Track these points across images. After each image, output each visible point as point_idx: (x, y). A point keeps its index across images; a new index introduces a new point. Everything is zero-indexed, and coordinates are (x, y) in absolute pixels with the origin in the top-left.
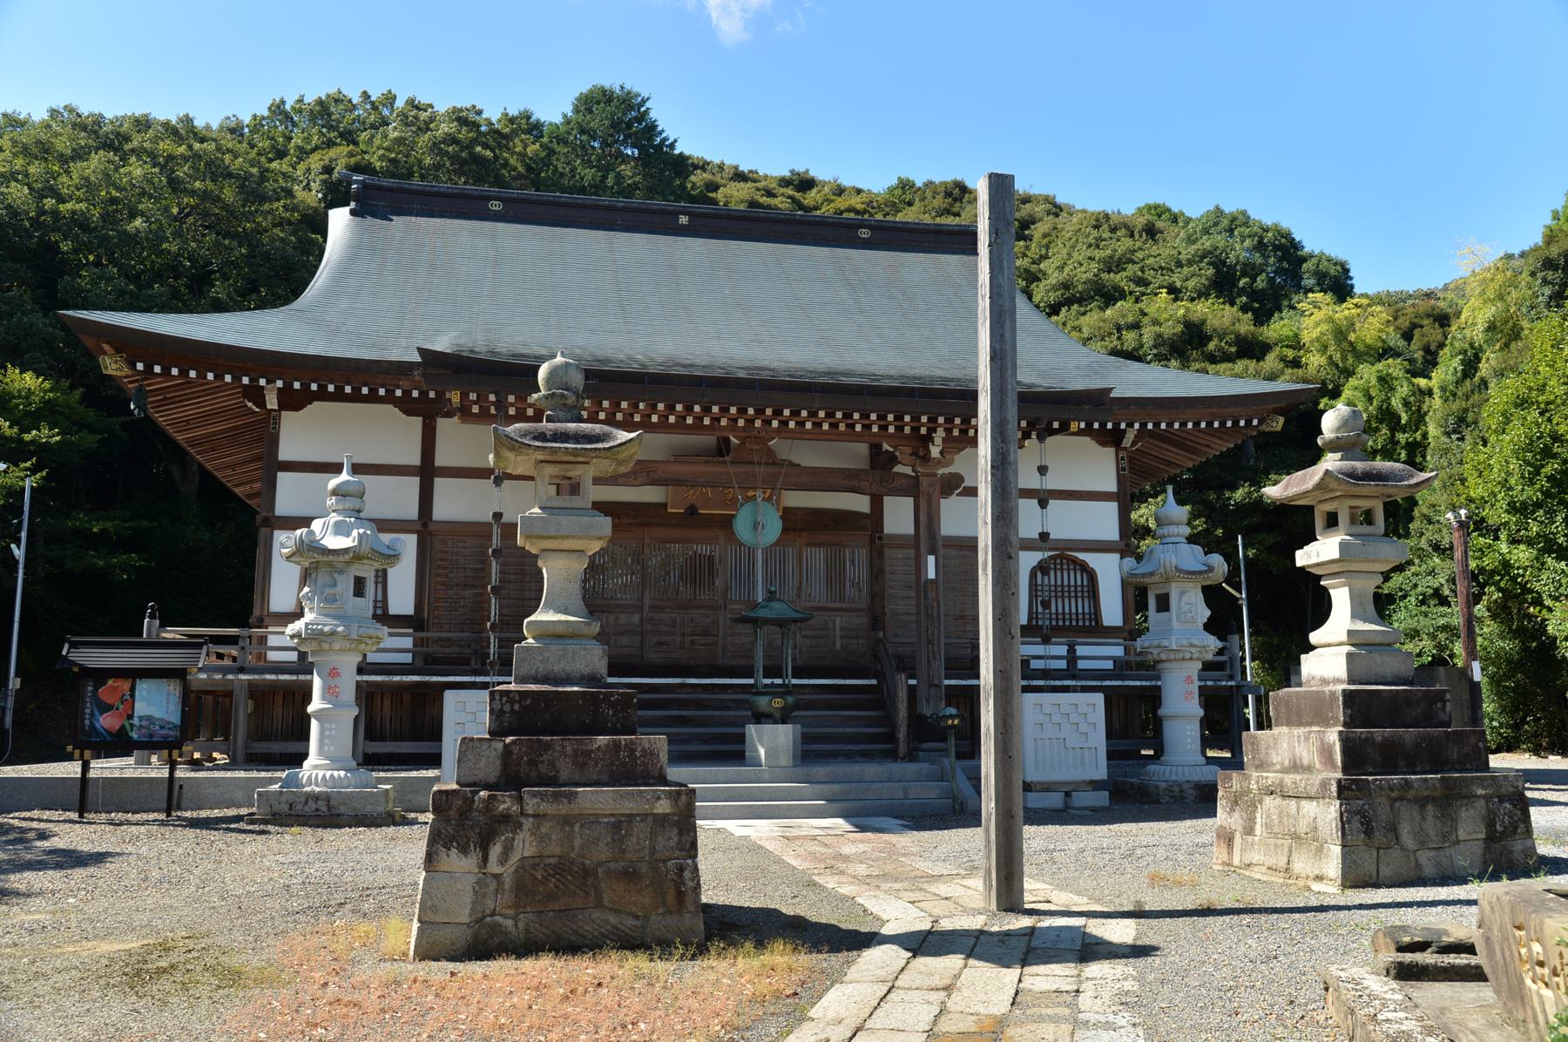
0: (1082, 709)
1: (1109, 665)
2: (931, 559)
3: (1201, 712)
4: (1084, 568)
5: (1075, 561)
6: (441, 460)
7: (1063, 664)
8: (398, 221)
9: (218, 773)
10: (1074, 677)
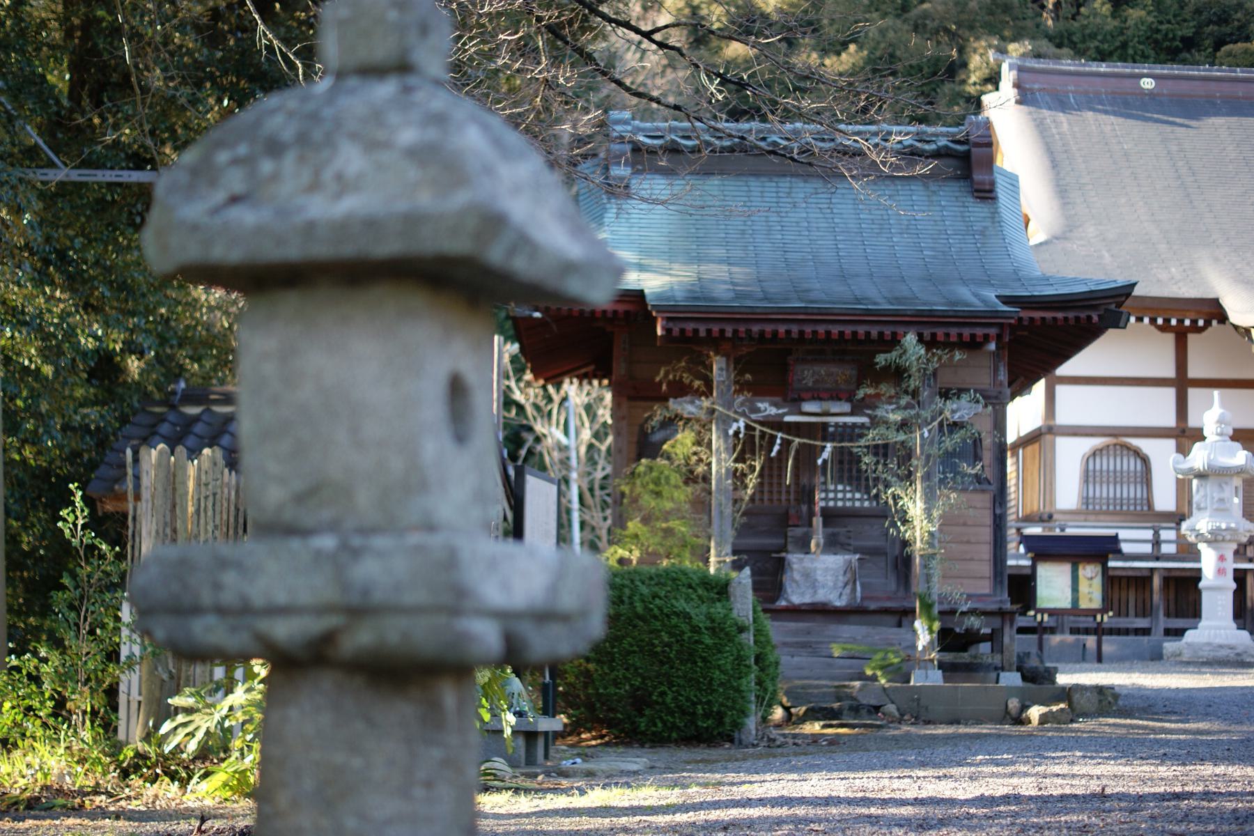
3: (1234, 586)
4: (1137, 453)
5: (1128, 448)
6: (1193, 372)
7: (1147, 549)
8: (715, 181)
9: (811, 748)
10: (1157, 559)
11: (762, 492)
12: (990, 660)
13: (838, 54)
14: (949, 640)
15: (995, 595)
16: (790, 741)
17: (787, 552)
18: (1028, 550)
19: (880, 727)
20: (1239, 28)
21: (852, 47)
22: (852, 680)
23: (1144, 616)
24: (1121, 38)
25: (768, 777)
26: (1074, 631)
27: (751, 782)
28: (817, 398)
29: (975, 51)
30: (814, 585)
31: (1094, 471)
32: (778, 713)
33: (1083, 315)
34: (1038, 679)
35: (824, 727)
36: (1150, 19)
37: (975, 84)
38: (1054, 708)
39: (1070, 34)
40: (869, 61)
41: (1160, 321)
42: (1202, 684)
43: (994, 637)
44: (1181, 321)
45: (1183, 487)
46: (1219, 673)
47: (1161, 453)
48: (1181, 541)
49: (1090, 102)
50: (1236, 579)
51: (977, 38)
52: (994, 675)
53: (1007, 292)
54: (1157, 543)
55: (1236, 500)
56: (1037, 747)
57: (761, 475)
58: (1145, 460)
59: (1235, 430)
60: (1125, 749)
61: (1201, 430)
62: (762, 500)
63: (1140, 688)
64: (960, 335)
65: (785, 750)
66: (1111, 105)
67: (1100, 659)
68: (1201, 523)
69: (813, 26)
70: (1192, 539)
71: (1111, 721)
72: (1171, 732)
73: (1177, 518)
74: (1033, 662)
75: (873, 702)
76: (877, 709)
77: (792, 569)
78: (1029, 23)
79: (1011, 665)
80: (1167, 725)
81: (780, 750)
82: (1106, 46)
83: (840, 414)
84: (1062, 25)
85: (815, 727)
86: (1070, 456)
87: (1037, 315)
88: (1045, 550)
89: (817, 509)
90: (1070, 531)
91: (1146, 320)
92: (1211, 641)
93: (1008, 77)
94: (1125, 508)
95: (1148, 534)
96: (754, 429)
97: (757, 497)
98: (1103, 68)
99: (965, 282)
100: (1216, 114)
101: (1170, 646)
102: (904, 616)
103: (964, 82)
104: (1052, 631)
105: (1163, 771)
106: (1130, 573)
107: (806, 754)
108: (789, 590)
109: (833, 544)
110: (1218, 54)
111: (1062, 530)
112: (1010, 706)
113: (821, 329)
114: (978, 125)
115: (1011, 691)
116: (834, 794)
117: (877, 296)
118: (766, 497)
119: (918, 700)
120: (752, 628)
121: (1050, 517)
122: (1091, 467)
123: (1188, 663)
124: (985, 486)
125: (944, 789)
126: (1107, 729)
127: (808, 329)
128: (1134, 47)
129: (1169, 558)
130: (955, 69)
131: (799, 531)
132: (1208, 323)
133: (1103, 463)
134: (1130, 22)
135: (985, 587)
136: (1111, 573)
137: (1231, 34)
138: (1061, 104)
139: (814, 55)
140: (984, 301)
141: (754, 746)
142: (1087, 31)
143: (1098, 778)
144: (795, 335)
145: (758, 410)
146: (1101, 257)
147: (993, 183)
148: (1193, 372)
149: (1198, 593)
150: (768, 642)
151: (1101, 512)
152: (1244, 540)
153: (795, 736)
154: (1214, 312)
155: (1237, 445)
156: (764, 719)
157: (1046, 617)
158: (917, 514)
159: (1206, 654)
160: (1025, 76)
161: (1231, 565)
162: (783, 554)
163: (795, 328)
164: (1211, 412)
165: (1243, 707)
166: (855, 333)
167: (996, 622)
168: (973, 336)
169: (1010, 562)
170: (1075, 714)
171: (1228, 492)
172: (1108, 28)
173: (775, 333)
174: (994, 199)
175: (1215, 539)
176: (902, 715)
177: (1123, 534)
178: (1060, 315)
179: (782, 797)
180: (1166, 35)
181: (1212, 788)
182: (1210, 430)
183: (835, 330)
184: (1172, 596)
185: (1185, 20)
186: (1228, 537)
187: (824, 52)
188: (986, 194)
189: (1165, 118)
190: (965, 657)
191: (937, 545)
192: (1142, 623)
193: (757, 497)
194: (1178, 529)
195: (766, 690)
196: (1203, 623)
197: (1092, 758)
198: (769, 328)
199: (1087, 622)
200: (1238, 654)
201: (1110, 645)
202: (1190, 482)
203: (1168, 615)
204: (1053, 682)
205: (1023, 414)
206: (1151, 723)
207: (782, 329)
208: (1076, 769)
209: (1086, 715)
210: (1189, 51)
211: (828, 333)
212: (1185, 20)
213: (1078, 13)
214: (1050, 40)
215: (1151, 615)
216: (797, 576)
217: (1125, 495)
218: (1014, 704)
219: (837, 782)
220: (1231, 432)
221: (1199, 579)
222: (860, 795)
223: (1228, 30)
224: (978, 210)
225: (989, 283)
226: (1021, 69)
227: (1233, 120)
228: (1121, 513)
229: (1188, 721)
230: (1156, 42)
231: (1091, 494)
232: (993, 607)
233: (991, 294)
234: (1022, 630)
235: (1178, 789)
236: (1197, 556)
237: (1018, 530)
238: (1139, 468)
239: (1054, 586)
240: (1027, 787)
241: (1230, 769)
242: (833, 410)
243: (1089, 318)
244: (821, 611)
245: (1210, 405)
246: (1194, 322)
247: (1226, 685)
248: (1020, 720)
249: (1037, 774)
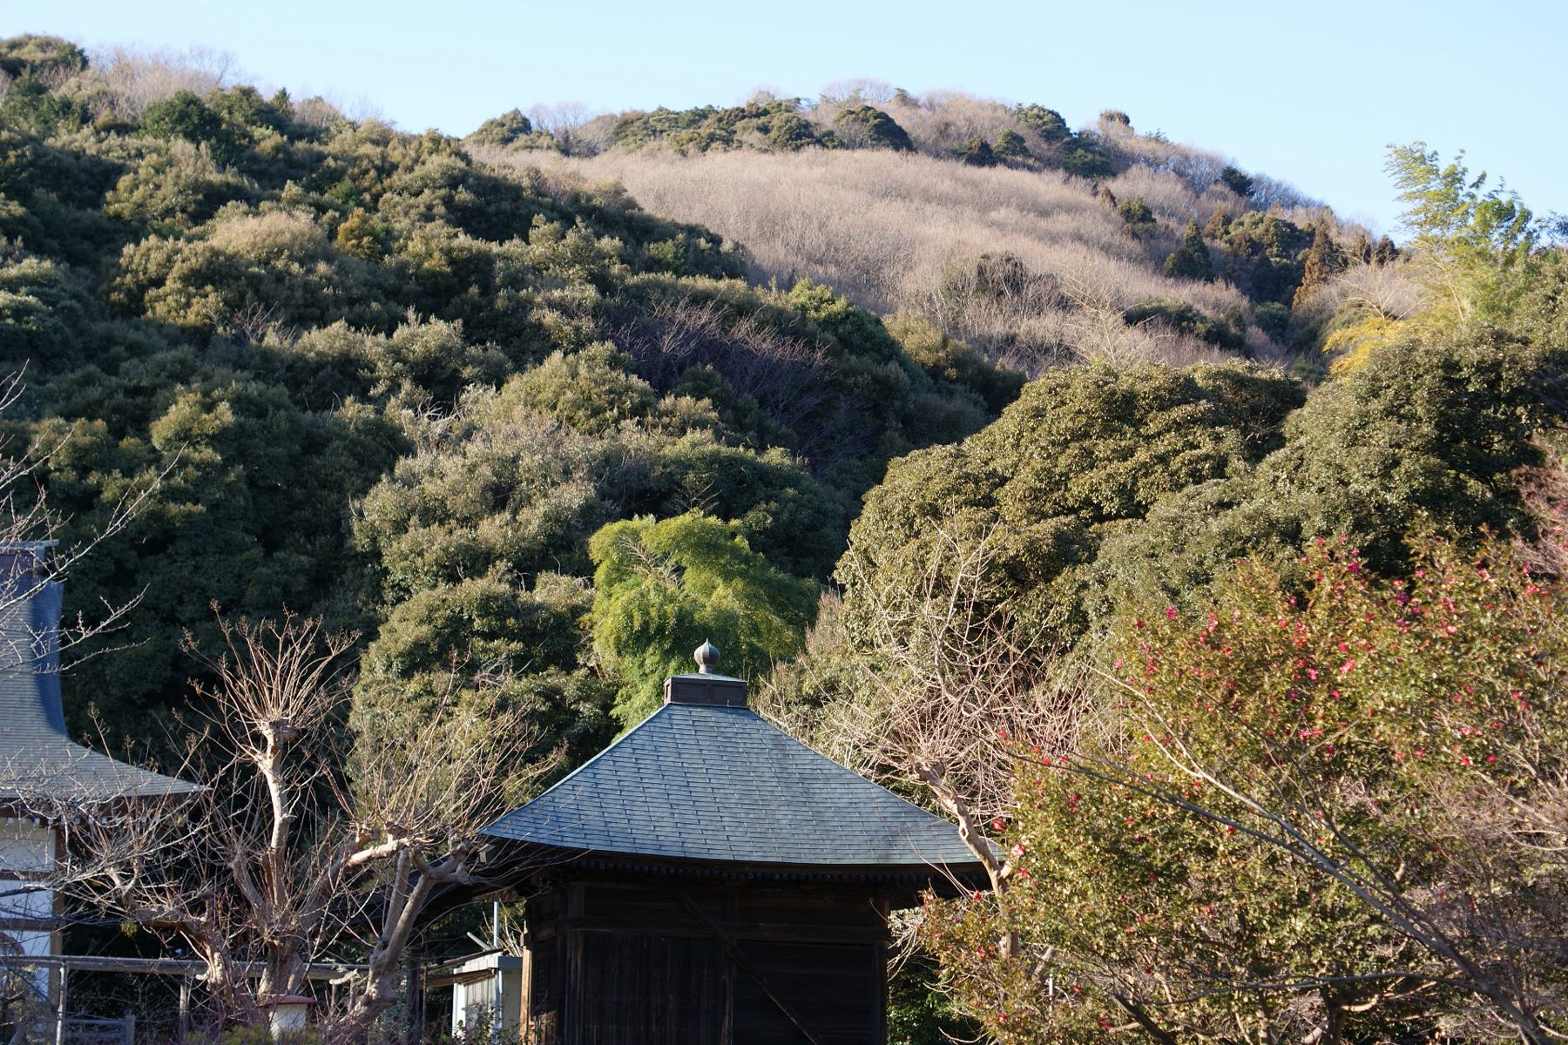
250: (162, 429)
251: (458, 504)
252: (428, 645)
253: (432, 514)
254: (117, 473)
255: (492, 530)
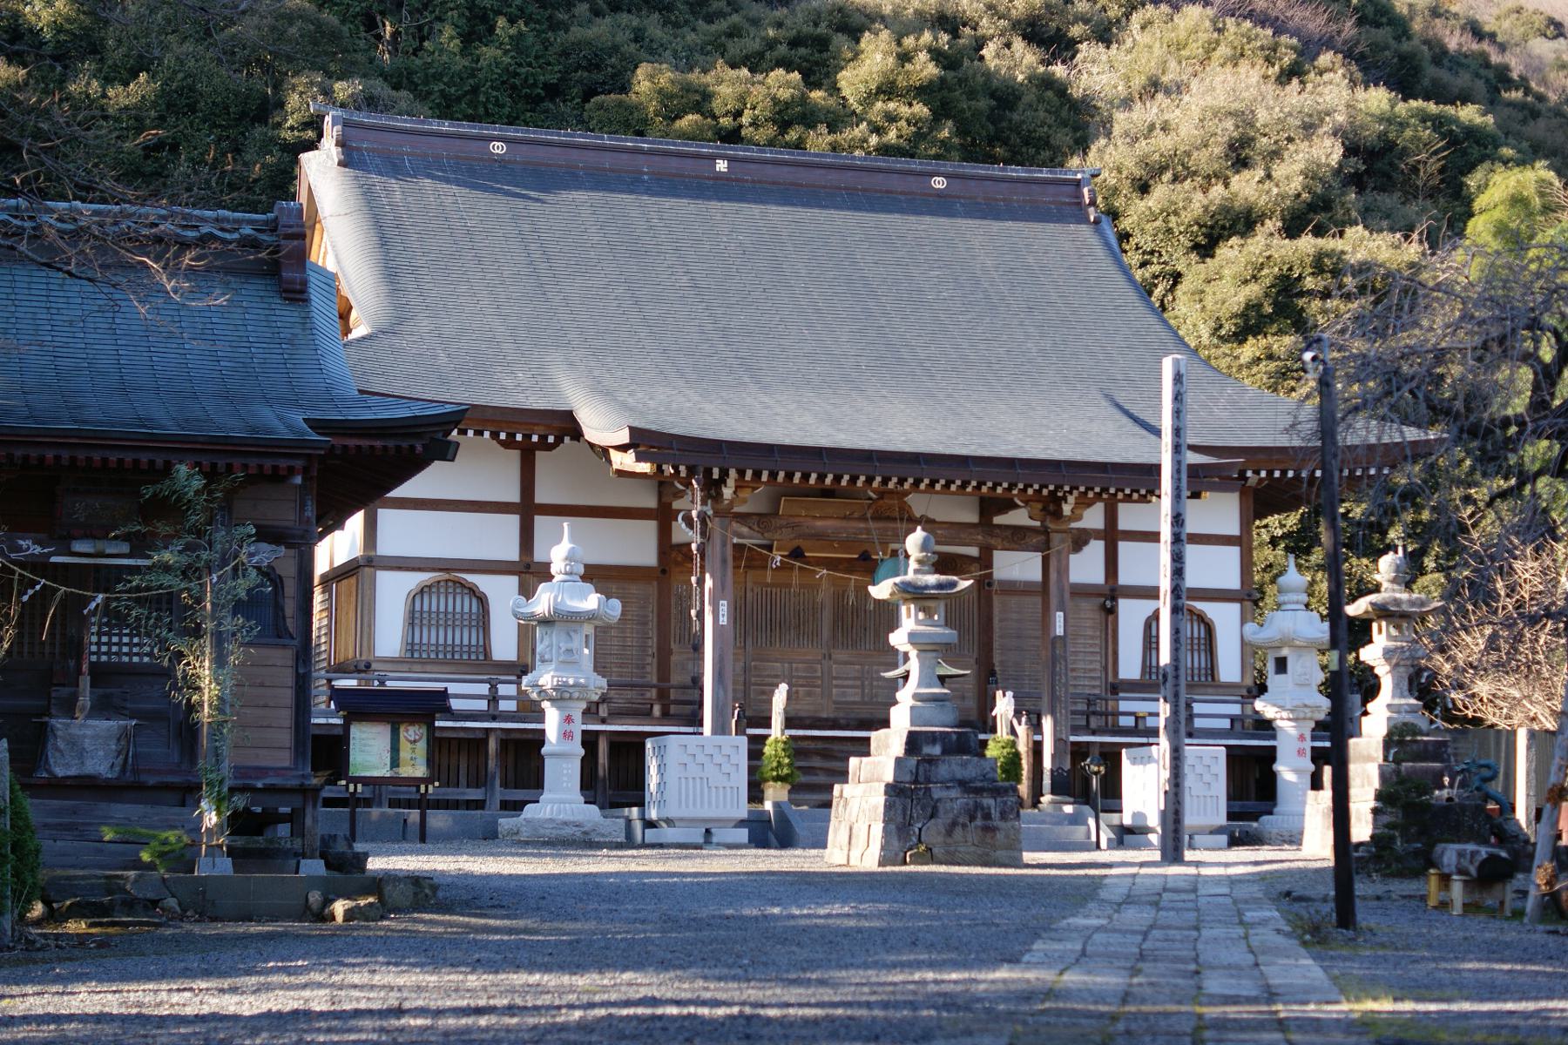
0: (1207, 761)
1: (1226, 724)
2: (1060, 616)
3: (582, 752)
4: (473, 591)
6: (541, 497)
7: (482, 705)
9: (76, 952)
10: (494, 718)
11: (21, 644)
12: (289, 845)
13: (126, 84)
14: (239, 823)
15: (296, 769)
16: (52, 943)
17: (50, 716)
18: (339, 707)
19: (157, 925)
20: (613, 76)
21: (143, 77)
22: (125, 869)
23: (477, 787)
24: (471, 81)
25: (29, 989)
26: (393, 803)
27: (12, 997)
28: (89, 535)
29: (294, 90)
30: (81, 754)
31: (422, 612)
32: (38, 909)
33: (405, 445)
34: (345, 868)
35: (91, 925)
36: (507, 60)
37: (292, 128)
38: (362, 903)
39: (411, 73)
40: (162, 94)
41: (503, 436)
42: (540, 870)
43: (295, 818)
44: (527, 437)
45: (527, 631)
46: (561, 856)
47: (500, 591)
48: (521, 697)
49: (429, 167)
50: (584, 744)
51: (296, 74)
52: (294, 862)
53: (317, 415)
54: (493, 699)
55: (586, 651)
56: (338, 949)
57: (20, 625)
58: (482, 600)
59: (587, 566)
60: (432, 954)
61: (548, 565)
62: (20, 653)
63: (468, 876)
64: (261, 467)
65: (47, 955)
66: (455, 172)
67: (423, 839)
68: (546, 678)
69: (94, 49)
70: (534, 696)
71: (427, 916)
72: (496, 930)
73: (520, 669)
74: (341, 847)
75: (151, 895)
76: (155, 903)
77: (55, 737)
78: (360, 57)
79: (313, 851)
80: (491, 922)
81: (40, 955)
82: (453, 90)
83: (116, 554)
84: (400, 59)
85: (76, 927)
86: (393, 594)
87: (352, 442)
88: (361, 706)
89: (85, 667)
90: (391, 685)
91: (487, 434)
92: (554, 816)
93: (331, 132)
94: (457, 656)
95: (484, 689)
96: (13, 572)
97: (16, 649)
98: (446, 126)
99: (267, 401)
100: (578, 188)
101: (506, 823)
102: (188, 794)
103: (279, 125)
104: (368, 803)
105: (473, 980)
106: (462, 735)
107: (70, 959)
108: (51, 761)
109: (103, 708)
110: (587, 106)
111: (382, 683)
112: (311, 899)
113: (97, 456)
114: (290, 210)
115: (313, 882)
116: (107, 1010)
117: (165, 418)
118: (26, 649)
119: (204, 892)
120: (8, 811)
121: (368, 666)
122: (418, 607)
123: (527, 843)
124: (287, 641)
125: (230, 1004)
126: (421, 928)
127: (81, 455)
128: (486, 93)
129: (508, 717)
130: (267, 109)
131: (65, 691)
132: (559, 440)
133: (433, 603)
134: (483, 63)
135: (284, 759)
136: (438, 734)
137: (604, 83)
138: (394, 167)
139: (95, 84)
140: (290, 427)
141: (10, 949)
142: (432, 71)
143: (400, 990)
144: (65, 462)
145: (19, 549)
146: (435, 357)
147: (305, 283)
148: (541, 497)
149: (541, 760)
150: (28, 826)
151: (429, 661)
152: (596, 698)
153: (57, 937)
154: (566, 426)
155: (589, 586)
156: (22, 917)
157: (359, 786)
158: (207, 681)
159: (548, 832)
160: (352, 132)
161: (578, 727)
162: (46, 719)
163: (66, 455)
164: (561, 547)
165: (581, 900)
166: (136, 462)
167: (297, 800)
168: (275, 468)
169: (315, 721)
170: (384, 909)
171: (577, 641)
172: (458, 68)
173: (42, 459)
174: (307, 301)
175: (561, 696)
176: (184, 911)
177: (453, 688)
178: (378, 443)
179: (48, 1014)
180: (526, 79)
181: (519, 1001)
182: (557, 567)
183: (113, 457)
184: (511, 759)
185: (549, 64)
186: (576, 695)
187: (108, 81)
188: (296, 294)
189: (518, 190)
190: (260, 841)
191: (228, 710)
192: (474, 794)
193: (16, 649)
194: (519, 684)
195: (24, 883)
196: (546, 796)
197: (396, 964)
198: (34, 453)
199: (408, 793)
200: (585, 833)
201: (439, 820)
202: (534, 628)
203: (505, 785)
204: (363, 869)
205: (338, 546)
206: (473, 920)
207: (50, 455)
208: (377, 979)
209: (397, 910)
210: (552, 100)
211: (105, 460)
212: (549, 64)
213: (421, 48)
214: (385, 79)
215: (485, 785)
216: (61, 744)
217: (457, 641)
218: (315, 897)
219: (109, 996)
220: (582, 571)
221: (542, 743)
222: (134, 1011)
223: (600, 77)
224: (287, 314)
225: (296, 404)
226: (346, 124)
227: (597, 195)
228: (452, 662)
229: (516, 917)
230: (514, 87)
231: (417, 640)
232: (294, 783)
233: (298, 418)
234: (329, 802)
235: (482, 1003)
236: (540, 716)
237: (329, 681)
238: (474, 609)
239: (370, 750)
240: (319, 1001)
241: (546, 978)
242: (108, 551)
243: (412, 448)
244: (88, 786)
245: (559, 541)
246: (543, 438)
247: (566, 870)
248: (324, 916)
249: (332, 985)
250: (854, 80)
251: (1203, 160)
252: (1260, 305)
253: (1174, 168)
254: (822, 128)
255: (1246, 187)
